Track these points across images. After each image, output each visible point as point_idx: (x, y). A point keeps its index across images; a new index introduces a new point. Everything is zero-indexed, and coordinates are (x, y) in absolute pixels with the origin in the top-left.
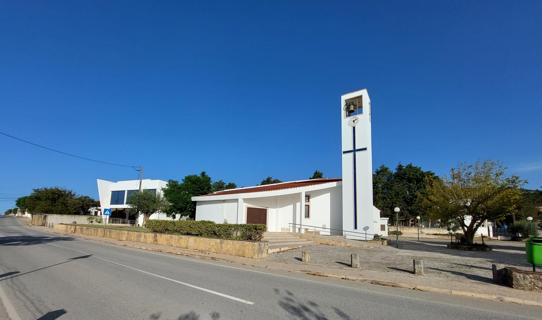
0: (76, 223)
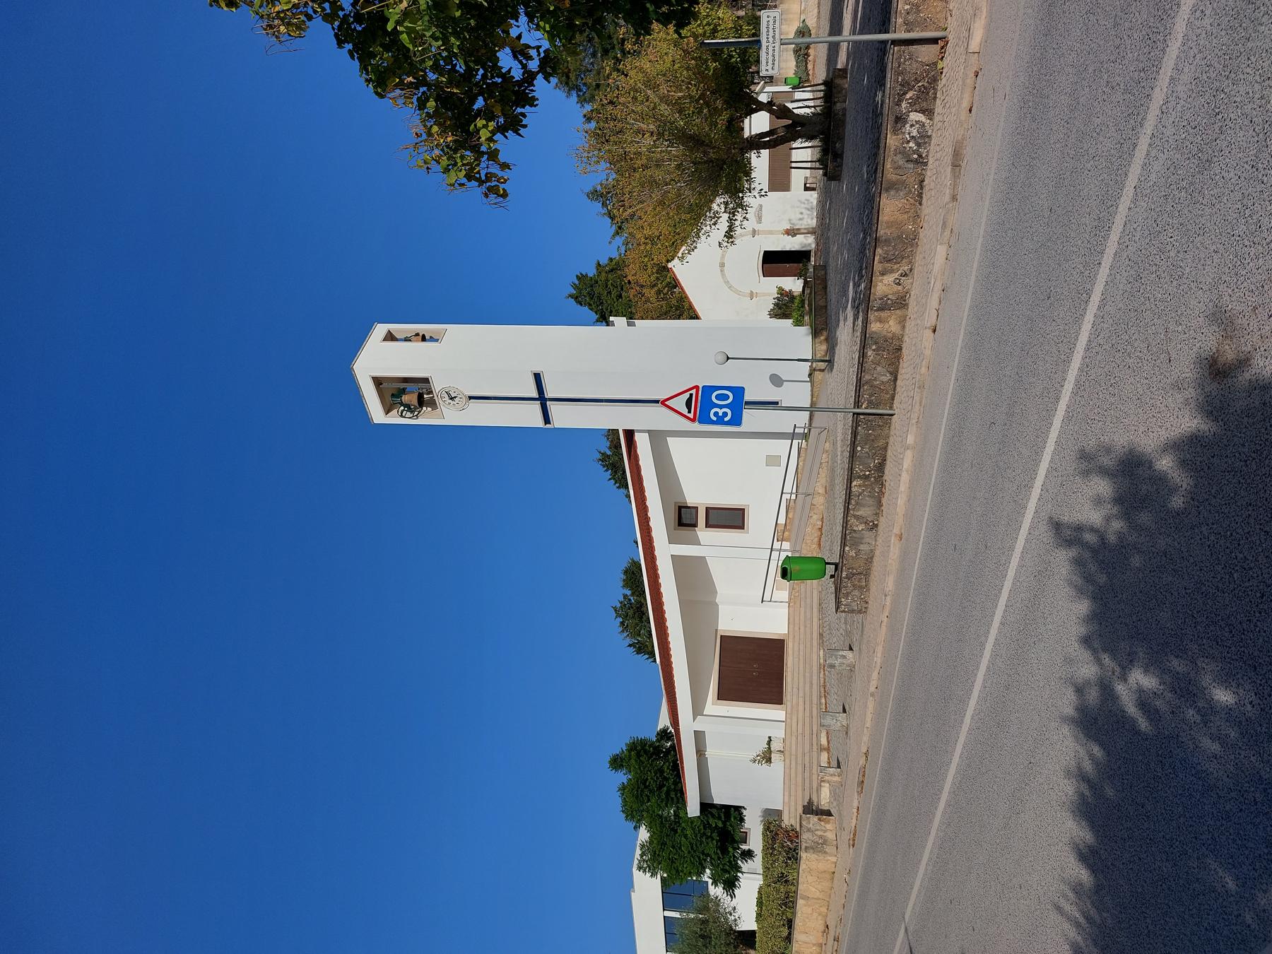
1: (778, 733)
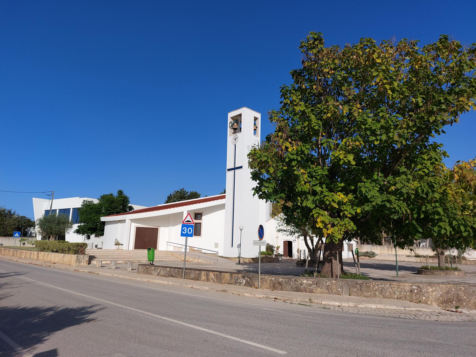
0: (2, 245)
1: (124, 248)
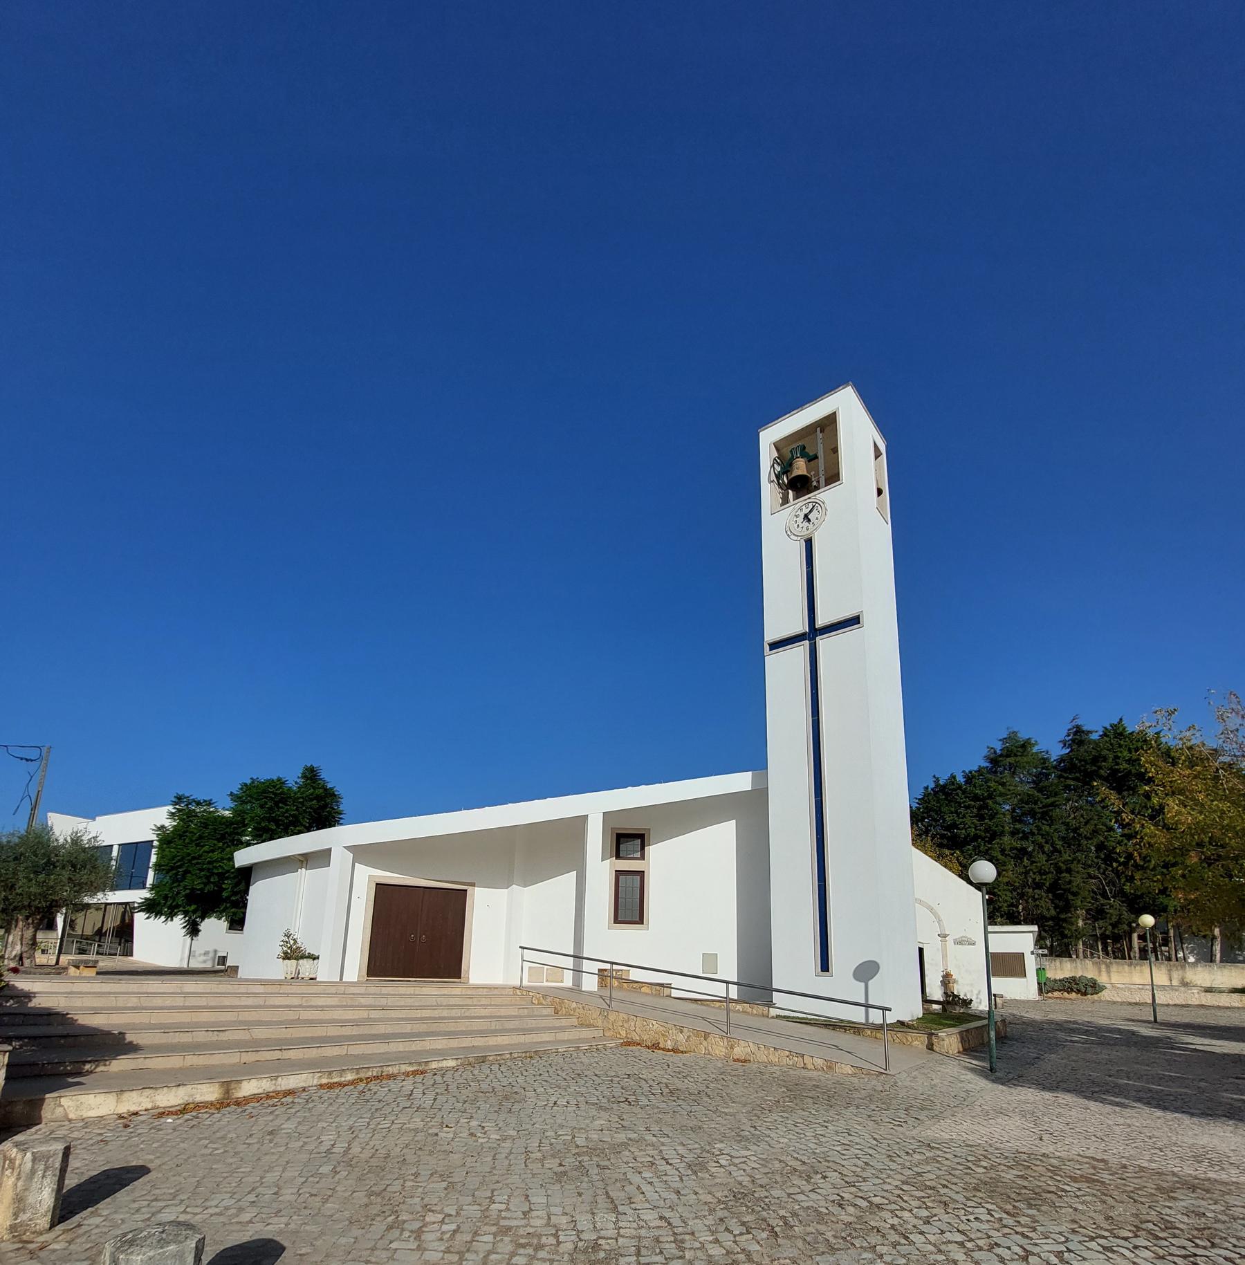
1: (325, 971)
